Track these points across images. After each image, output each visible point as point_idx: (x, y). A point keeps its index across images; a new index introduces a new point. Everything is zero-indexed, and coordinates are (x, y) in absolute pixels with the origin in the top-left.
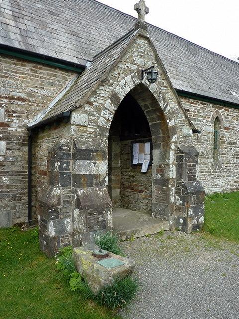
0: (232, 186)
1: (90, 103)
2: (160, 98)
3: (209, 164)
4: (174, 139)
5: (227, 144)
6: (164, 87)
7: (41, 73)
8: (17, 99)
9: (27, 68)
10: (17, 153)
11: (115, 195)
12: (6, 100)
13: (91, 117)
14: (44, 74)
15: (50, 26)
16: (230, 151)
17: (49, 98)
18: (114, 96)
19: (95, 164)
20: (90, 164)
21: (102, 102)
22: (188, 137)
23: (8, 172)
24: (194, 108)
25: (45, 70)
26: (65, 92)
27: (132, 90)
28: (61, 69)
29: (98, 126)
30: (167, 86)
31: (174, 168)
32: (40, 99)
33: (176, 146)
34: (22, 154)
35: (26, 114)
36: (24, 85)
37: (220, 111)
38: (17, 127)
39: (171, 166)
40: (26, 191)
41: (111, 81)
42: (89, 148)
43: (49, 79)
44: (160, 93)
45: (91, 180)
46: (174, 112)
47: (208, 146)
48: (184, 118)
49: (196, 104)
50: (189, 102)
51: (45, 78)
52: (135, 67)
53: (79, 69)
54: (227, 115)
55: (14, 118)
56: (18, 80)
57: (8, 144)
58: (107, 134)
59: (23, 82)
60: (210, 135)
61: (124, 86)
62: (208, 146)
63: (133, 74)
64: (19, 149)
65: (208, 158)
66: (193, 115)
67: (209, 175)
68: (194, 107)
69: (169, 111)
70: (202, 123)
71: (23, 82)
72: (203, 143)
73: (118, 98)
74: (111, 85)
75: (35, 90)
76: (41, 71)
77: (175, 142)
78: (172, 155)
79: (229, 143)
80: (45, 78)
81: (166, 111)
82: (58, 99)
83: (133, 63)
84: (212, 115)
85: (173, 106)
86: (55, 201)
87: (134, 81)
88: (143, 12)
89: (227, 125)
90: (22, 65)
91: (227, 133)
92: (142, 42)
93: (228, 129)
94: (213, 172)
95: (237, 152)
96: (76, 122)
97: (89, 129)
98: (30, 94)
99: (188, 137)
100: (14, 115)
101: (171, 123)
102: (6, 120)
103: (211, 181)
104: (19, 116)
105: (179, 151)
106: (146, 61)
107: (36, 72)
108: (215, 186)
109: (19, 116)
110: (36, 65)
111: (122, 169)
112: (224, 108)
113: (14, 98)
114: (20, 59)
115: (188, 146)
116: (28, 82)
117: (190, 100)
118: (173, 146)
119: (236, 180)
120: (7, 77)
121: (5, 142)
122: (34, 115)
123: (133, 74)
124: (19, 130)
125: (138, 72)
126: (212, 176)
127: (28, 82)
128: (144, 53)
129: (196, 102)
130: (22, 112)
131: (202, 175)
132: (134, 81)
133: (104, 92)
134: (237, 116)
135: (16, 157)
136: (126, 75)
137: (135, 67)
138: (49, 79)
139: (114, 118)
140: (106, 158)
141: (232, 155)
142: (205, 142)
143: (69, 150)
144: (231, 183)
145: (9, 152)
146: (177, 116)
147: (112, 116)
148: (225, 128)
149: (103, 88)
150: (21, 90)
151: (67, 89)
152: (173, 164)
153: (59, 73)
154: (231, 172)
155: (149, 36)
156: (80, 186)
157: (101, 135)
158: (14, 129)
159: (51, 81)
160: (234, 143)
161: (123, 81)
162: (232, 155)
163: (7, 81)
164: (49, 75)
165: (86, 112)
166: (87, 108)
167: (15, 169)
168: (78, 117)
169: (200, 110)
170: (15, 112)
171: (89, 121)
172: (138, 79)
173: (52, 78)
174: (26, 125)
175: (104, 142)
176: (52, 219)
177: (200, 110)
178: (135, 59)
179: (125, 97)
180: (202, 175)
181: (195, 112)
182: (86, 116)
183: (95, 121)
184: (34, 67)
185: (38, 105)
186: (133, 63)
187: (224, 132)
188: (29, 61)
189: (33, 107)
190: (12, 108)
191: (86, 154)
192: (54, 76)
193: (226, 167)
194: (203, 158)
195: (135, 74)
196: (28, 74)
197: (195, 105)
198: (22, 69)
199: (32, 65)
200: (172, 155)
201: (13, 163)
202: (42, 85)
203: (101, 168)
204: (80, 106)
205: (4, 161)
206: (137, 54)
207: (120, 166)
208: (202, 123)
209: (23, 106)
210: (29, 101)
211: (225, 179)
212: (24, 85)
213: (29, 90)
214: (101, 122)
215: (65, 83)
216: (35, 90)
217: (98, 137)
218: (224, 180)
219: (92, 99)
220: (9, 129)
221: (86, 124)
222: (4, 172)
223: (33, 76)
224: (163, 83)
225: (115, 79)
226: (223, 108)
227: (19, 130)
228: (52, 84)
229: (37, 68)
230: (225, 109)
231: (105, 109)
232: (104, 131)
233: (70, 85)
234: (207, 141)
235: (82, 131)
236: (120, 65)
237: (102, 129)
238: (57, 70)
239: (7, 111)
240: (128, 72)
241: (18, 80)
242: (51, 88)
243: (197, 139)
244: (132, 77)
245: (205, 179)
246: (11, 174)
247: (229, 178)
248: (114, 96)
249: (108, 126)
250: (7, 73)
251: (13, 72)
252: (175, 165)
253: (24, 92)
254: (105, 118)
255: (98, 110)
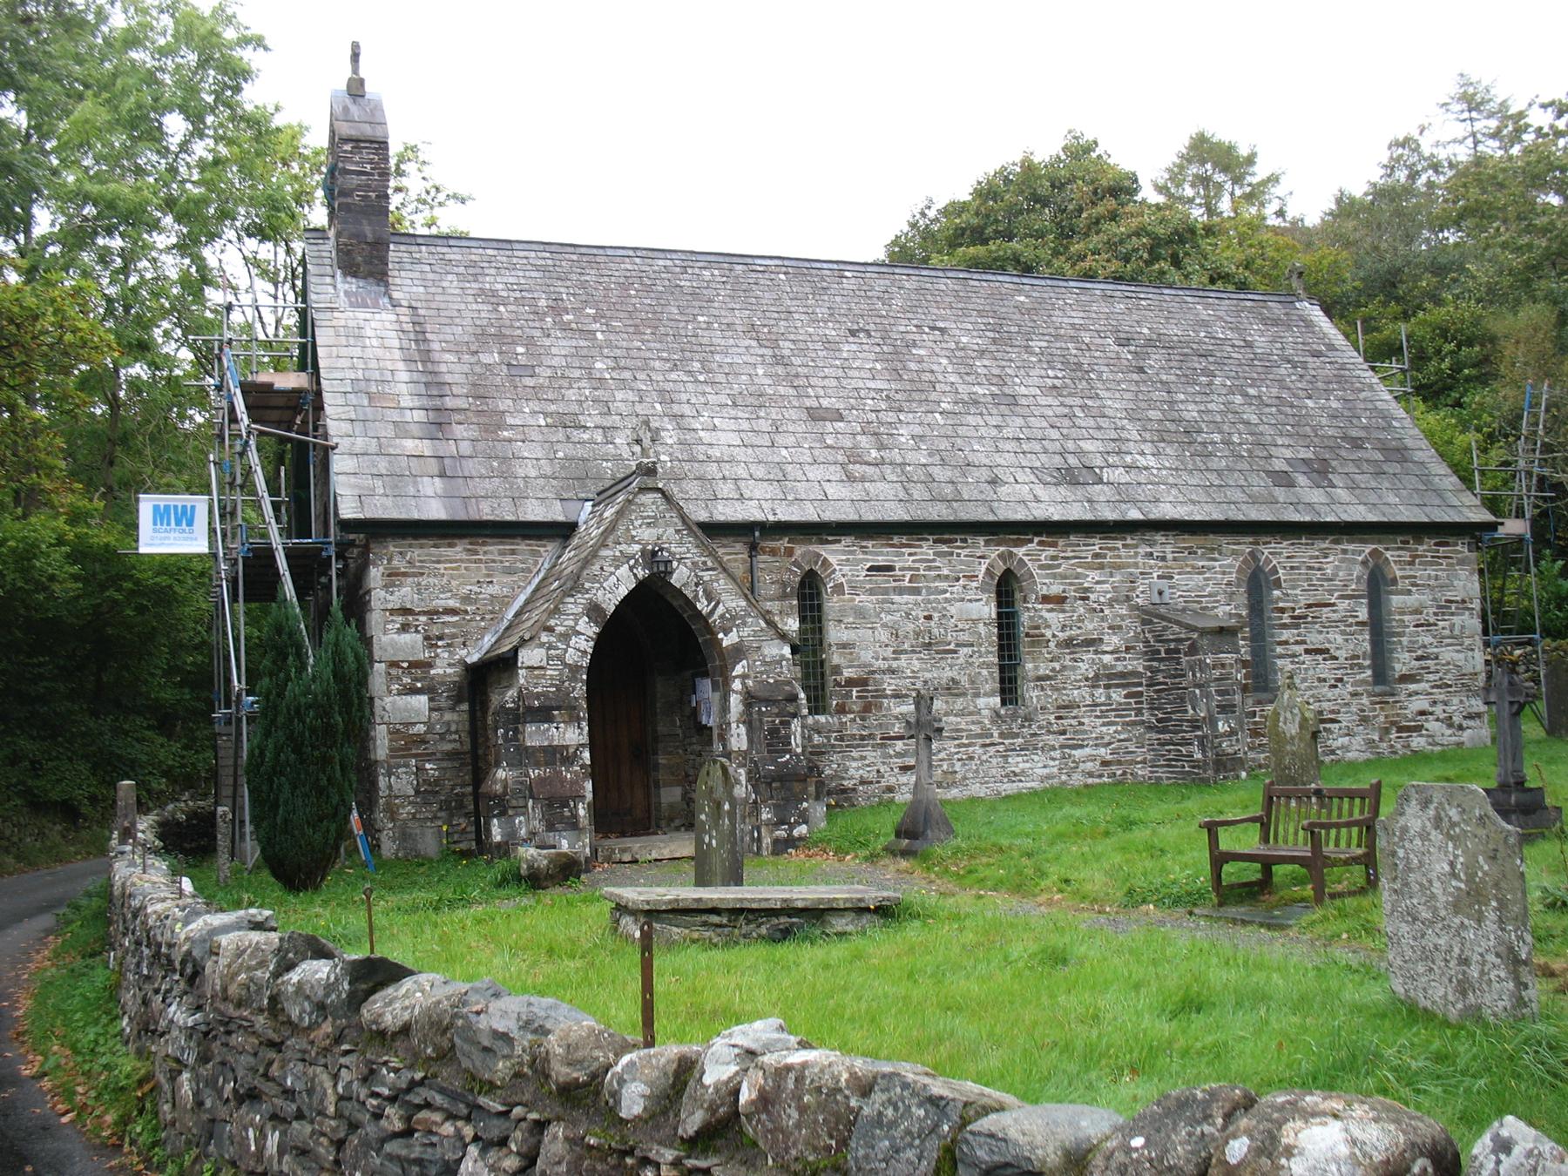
0: (1091, 774)
1: (550, 630)
2: (696, 596)
3: (985, 712)
4: (739, 669)
5: (1058, 645)
6: (708, 570)
7: (485, 553)
8: (443, 613)
9: (458, 549)
10: (448, 716)
11: (671, 800)
12: (423, 619)
13: (552, 652)
14: (492, 553)
15: (510, 421)
16: (1074, 669)
17: (505, 601)
18: (594, 610)
19: (557, 728)
20: (548, 730)
21: (572, 623)
22: (780, 662)
23: (434, 754)
24: (912, 558)
25: (493, 544)
26: (536, 581)
27: (631, 593)
28: (526, 537)
29: (566, 665)
30: (716, 565)
31: (743, 729)
32: (485, 605)
33: (743, 684)
34: (457, 718)
35: (462, 640)
36: (454, 583)
37: (1020, 552)
38: (445, 668)
39: (734, 726)
40: (470, 789)
41: (587, 585)
42: (547, 703)
43: (501, 562)
44: (697, 585)
45: (556, 755)
46: (733, 618)
47: (977, 661)
48: (763, 625)
49: (921, 547)
50: (893, 546)
51: (494, 561)
52: (637, 547)
53: (563, 531)
54: (1054, 558)
55: (439, 650)
56: (443, 575)
57: (431, 700)
58: (585, 677)
59: (452, 577)
60: (981, 628)
61: (615, 586)
62: (977, 661)
63: (632, 562)
64: (452, 709)
65: (977, 695)
66: (907, 579)
67: (984, 746)
68: (910, 555)
69: (722, 616)
70: (948, 595)
71: (452, 577)
72: (955, 652)
73: (603, 611)
74: (587, 591)
75: (475, 589)
76: (486, 548)
77: (744, 677)
78: (735, 702)
79: (1068, 643)
80: (494, 561)
81: (716, 616)
82: (522, 598)
83: (633, 540)
84: (983, 568)
85: (734, 605)
86: (498, 788)
87: (635, 575)
88: (647, 442)
89: (1056, 589)
90: (450, 545)
91: (1053, 614)
92: (648, 498)
93: (1060, 600)
94: (1002, 735)
95: (1105, 667)
96: (528, 663)
97: (549, 672)
98: (466, 599)
99: (780, 662)
100: (440, 643)
101: (728, 640)
102: (425, 655)
103: (994, 761)
104: (449, 645)
105: (750, 699)
106: (661, 530)
107: (477, 553)
108: (1013, 776)
109: (449, 645)
110: (473, 540)
111: (685, 737)
112: (1036, 540)
113: (437, 613)
114: (443, 536)
115: (776, 681)
116: (461, 576)
117: (896, 540)
118: (737, 685)
119: (1109, 758)
120: (423, 574)
121: (426, 697)
122: (477, 639)
123: (632, 562)
124: (449, 671)
125: (643, 555)
126: (1001, 748)
127: (461, 576)
128: (655, 517)
129: (919, 540)
130: (454, 636)
131: (959, 746)
132: (635, 575)
133: (576, 605)
134: (1096, 556)
135: (448, 724)
136: (617, 567)
137: (637, 547)
138: (501, 562)
139: (595, 648)
140: (579, 720)
141: (1087, 679)
142: (965, 650)
143: (518, 709)
144: (1089, 766)
145: (435, 715)
146: (744, 624)
147: (592, 644)
148: (1046, 599)
149: (572, 600)
150: (449, 594)
151: (541, 575)
152: (738, 722)
153: (522, 546)
154: (1085, 732)
155: (660, 485)
156: (537, 765)
157: (573, 679)
158: (441, 671)
159: (507, 564)
160: (1089, 643)
161: (613, 579)
162: (1087, 679)
163: (424, 581)
164: (502, 553)
165: (542, 645)
166: (544, 638)
167: (448, 747)
168: (529, 656)
169: (934, 561)
170: (440, 638)
171: (549, 658)
172: (643, 569)
173: (509, 558)
174: (462, 662)
175: (579, 690)
176: (495, 816)
177: (934, 561)
178: (634, 533)
179: (617, 607)
180: (959, 746)
181: (918, 569)
182: (543, 651)
183: (561, 658)
184: (471, 544)
185: (483, 619)
186: (633, 540)
187: (1045, 614)
188: (462, 537)
189: (474, 624)
190: (435, 631)
191: (543, 714)
192: (513, 552)
193: (1057, 718)
194: (957, 695)
195: (637, 561)
196: (462, 561)
197: (913, 550)
198: (445, 551)
199: (467, 541)
200: (735, 702)
201: (442, 736)
202: (488, 576)
203: (573, 735)
204: (531, 638)
205: (426, 733)
206: (640, 522)
207: (680, 732)
208: (948, 595)
209: (454, 625)
210: (466, 612)
211: (1057, 754)
212: (454, 583)
213: (465, 590)
214: (571, 657)
215: (536, 563)
216: (475, 589)
217: (566, 684)
218: (1053, 759)
219: (552, 622)
220: (432, 672)
221: (544, 663)
222: (428, 754)
223: (470, 561)
224: (704, 563)
225: (594, 579)
226: (1031, 541)
227: (449, 671)
228: (509, 571)
229: (478, 544)
230: (1041, 543)
231: (579, 633)
232: (577, 672)
233: (546, 566)
234: (972, 645)
235: (537, 677)
236: (604, 553)
237: (574, 669)
238: (518, 540)
239: (427, 638)
240: (617, 562)
241: (443, 575)
242: (508, 579)
243: (930, 644)
244: (631, 569)
245: (971, 758)
246: (439, 756)
247: (1077, 753)
248: (594, 610)
249: (585, 662)
250: (421, 567)
251: (434, 562)
252: (744, 723)
253: (454, 596)
254: (579, 650)
255: (565, 637)
